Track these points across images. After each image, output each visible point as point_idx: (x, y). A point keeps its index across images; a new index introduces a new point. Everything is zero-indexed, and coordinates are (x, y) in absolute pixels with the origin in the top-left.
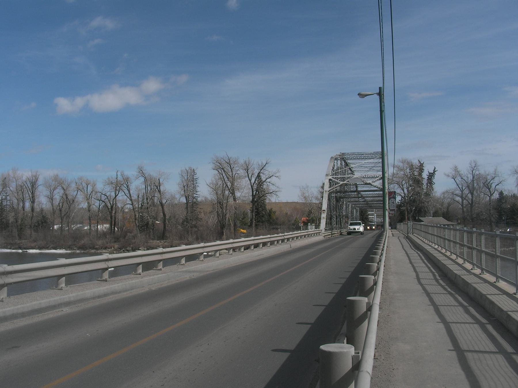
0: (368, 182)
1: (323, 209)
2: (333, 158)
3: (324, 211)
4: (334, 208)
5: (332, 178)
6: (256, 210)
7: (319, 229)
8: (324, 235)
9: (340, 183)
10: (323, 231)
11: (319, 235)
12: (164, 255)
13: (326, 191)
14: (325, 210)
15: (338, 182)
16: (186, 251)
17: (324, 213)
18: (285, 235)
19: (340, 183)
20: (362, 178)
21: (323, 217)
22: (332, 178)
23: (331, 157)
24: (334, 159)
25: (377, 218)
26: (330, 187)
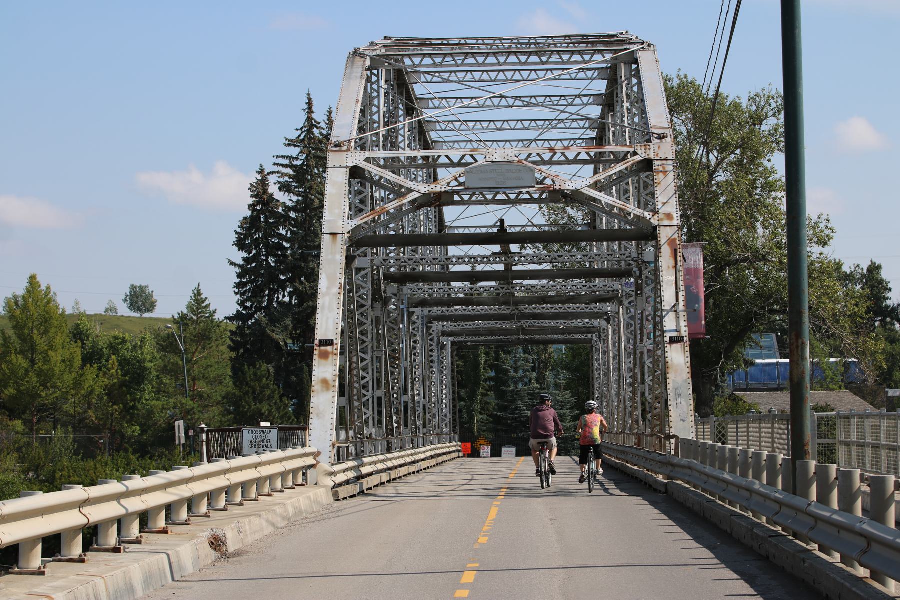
0: (569, 187)
1: (321, 333)
2: (363, 56)
3: (329, 349)
4: (431, 340)
5: (367, 160)
6: (631, 389)
7: (308, 450)
8: (329, 482)
9: (410, 191)
10: (326, 462)
11: (305, 479)
12: (145, 497)
13: (334, 235)
14: (330, 343)
15: (401, 187)
16: (273, 466)
17: (324, 356)
18: (128, 494)
19: (410, 191)
20: (535, 163)
21: (325, 382)
22: (367, 160)
23: (352, 51)
24: (368, 63)
25: (481, 456)
26: (356, 210)
